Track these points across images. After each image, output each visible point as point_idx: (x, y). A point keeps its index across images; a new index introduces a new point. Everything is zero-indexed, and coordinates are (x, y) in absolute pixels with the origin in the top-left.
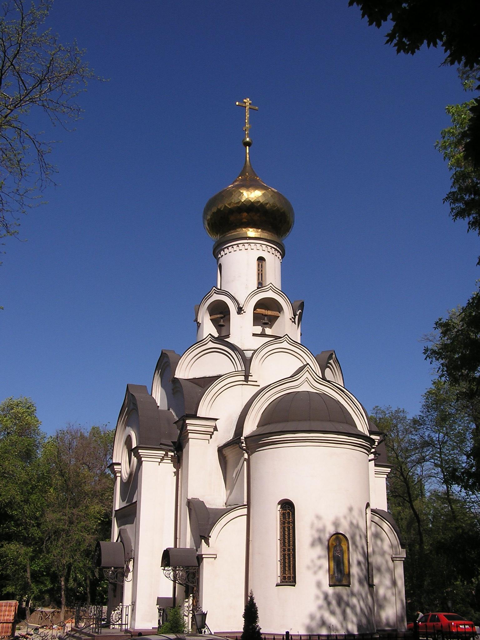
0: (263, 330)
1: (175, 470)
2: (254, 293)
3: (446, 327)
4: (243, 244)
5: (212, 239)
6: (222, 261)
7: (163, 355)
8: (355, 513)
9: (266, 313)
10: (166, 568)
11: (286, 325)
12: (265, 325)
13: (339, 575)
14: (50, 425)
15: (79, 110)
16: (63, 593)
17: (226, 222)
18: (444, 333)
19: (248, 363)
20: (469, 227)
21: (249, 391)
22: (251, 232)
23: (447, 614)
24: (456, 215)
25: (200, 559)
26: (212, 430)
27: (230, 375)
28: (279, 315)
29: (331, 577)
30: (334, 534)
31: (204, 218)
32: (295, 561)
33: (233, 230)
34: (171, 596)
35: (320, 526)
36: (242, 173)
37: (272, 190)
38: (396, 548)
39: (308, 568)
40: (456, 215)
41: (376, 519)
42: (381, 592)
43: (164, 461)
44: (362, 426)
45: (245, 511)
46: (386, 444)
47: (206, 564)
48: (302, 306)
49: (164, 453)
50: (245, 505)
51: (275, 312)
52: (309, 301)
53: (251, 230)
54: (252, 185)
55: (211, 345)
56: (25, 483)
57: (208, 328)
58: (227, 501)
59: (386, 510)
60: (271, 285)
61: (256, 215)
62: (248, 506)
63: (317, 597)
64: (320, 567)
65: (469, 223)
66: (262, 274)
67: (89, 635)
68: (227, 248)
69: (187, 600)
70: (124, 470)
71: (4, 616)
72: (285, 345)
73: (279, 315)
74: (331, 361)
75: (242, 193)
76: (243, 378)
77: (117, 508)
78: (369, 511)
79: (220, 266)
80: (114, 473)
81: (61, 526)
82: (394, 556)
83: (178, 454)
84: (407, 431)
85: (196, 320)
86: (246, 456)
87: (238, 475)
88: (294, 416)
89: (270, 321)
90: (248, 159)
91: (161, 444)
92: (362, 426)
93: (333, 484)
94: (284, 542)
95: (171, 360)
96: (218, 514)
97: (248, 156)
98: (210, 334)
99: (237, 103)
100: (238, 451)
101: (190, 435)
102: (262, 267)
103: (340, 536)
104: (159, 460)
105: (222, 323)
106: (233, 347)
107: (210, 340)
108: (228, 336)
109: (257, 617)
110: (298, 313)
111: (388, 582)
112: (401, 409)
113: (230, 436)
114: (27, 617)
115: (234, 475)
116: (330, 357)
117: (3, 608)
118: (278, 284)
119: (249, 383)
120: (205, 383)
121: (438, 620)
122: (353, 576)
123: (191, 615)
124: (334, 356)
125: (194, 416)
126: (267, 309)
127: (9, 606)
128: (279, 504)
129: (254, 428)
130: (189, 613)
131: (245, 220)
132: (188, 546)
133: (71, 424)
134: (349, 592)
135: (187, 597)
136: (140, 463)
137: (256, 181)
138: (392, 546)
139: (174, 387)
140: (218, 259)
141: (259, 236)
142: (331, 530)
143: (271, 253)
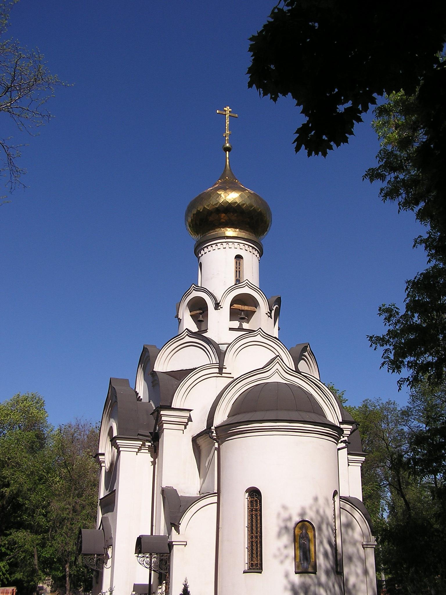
1: (152, 460)
3: (389, 312)
5: (194, 238)
6: (202, 259)
7: (145, 350)
8: (321, 501)
9: (242, 309)
10: (140, 555)
11: (262, 319)
12: (242, 319)
13: (305, 563)
15: (49, 116)
17: (207, 223)
18: (388, 319)
19: (222, 355)
20: (400, 208)
21: (224, 382)
22: (230, 232)
24: (386, 196)
25: (170, 546)
26: (186, 420)
27: (204, 368)
28: (256, 310)
29: (297, 567)
30: (300, 522)
31: (186, 219)
32: (261, 548)
33: (212, 230)
34: (148, 583)
35: (285, 515)
36: (223, 177)
39: (275, 556)
41: (348, 507)
42: (352, 580)
43: (141, 451)
44: (333, 415)
45: (215, 499)
46: (363, 434)
47: (177, 553)
48: (278, 301)
49: (141, 443)
50: (215, 493)
51: (251, 308)
53: (229, 229)
54: (234, 187)
55: (188, 339)
57: (189, 323)
58: (201, 489)
60: (247, 281)
62: (218, 494)
64: (287, 557)
65: (399, 204)
66: (239, 272)
68: (207, 247)
69: (160, 587)
70: (107, 461)
72: (259, 338)
73: (256, 310)
74: (306, 354)
75: (220, 195)
76: (217, 370)
77: (102, 496)
78: (337, 498)
79: (201, 265)
82: (364, 543)
83: (155, 444)
84: (397, 423)
85: (177, 316)
86: (216, 445)
87: (210, 464)
88: (264, 407)
89: (248, 316)
90: (228, 163)
91: (138, 434)
92: (333, 415)
93: (304, 473)
96: (191, 501)
97: (228, 161)
99: (218, 112)
100: (210, 441)
101: (165, 426)
102: (239, 265)
103: (306, 523)
104: (137, 450)
105: (201, 318)
106: (208, 341)
107: (187, 335)
108: (206, 331)
110: (274, 308)
111: (360, 571)
113: (203, 427)
115: (207, 464)
116: (305, 349)
119: (223, 375)
120: (180, 375)
122: (320, 565)
124: (308, 348)
126: (245, 304)
128: (247, 491)
129: (225, 418)
131: (223, 220)
132: (162, 534)
134: (316, 581)
135: (160, 583)
136: (119, 452)
137: (236, 183)
138: (363, 535)
139: (153, 379)
140: (199, 258)
141: (236, 236)
142: (296, 519)
143: (248, 251)
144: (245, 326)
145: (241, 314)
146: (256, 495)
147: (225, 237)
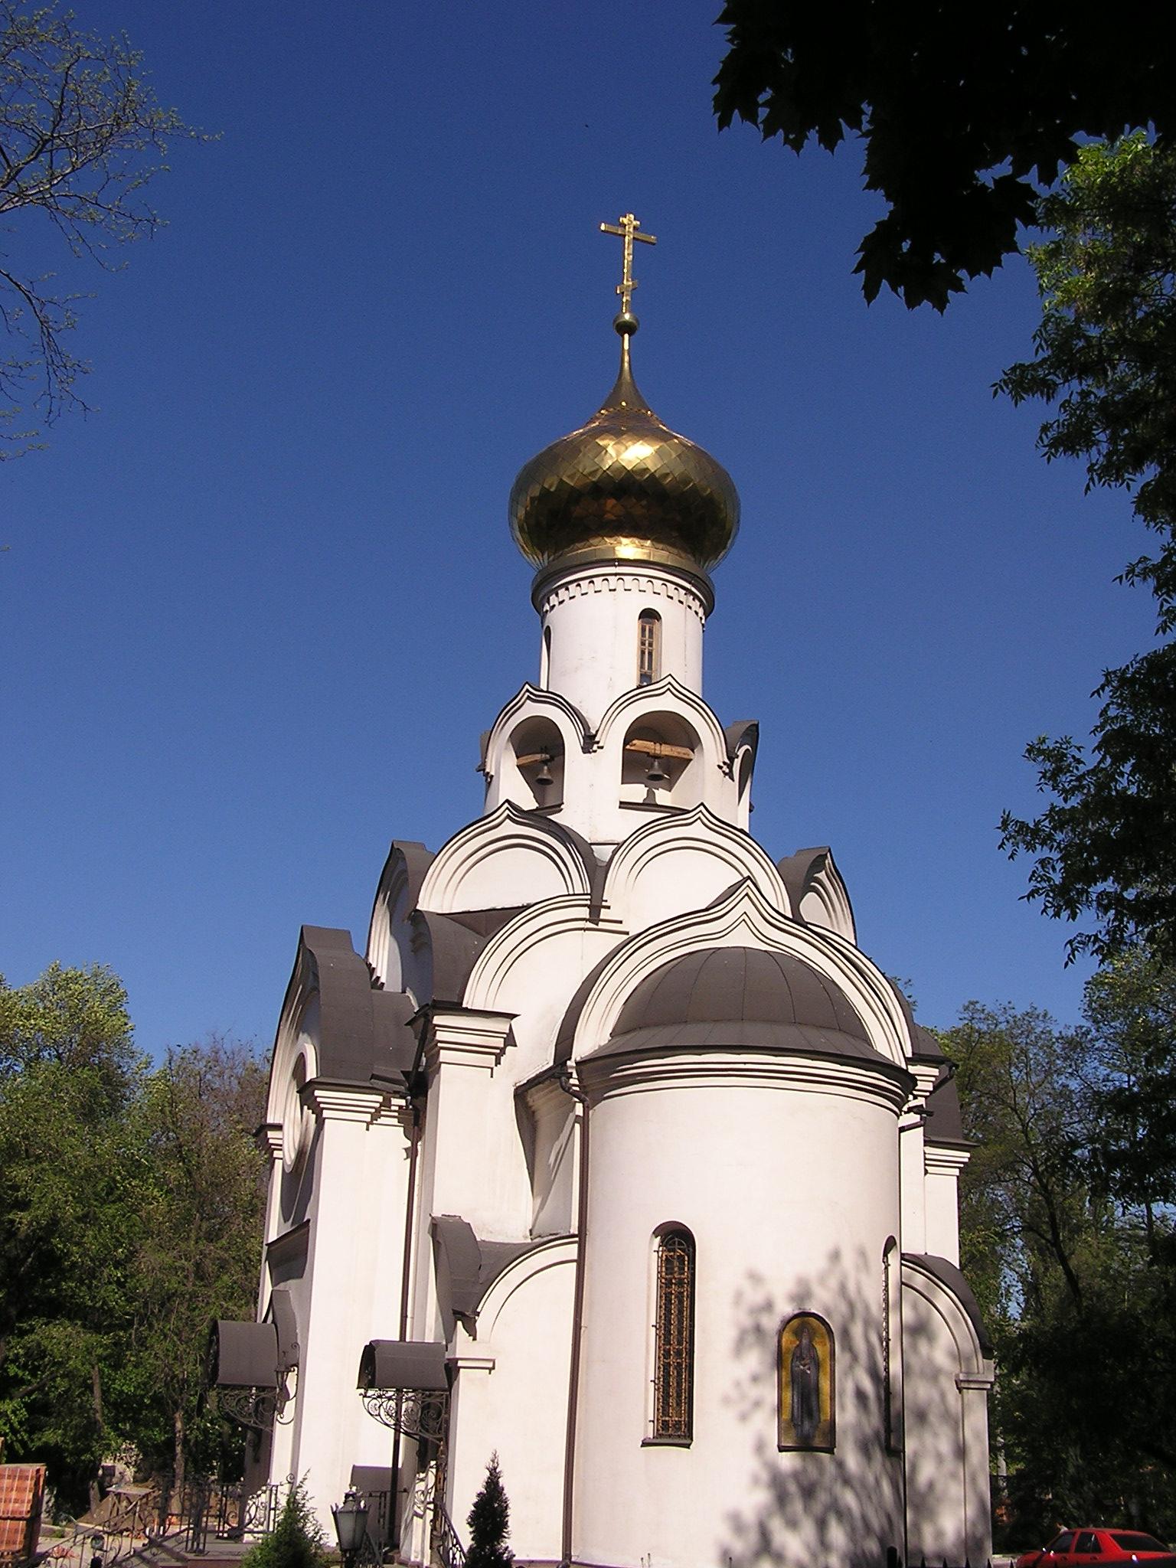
0: (651, 794)
1: (408, 1144)
2: (628, 699)
3: (1055, 761)
4: (605, 577)
7: (395, 855)
8: (848, 1260)
9: (655, 751)
10: (370, 1393)
11: (707, 781)
12: (654, 780)
13: (806, 1424)
14: (157, 1038)
16: (179, 1449)
17: (567, 522)
18: (1052, 777)
21: (602, 944)
22: (628, 548)
23: (1120, 1532)
24: (1055, 444)
25: (452, 1370)
26: (500, 1042)
27: (550, 904)
30: (795, 1316)
31: (512, 512)
34: (390, 1465)
35: (755, 1297)
36: (612, 401)
37: (681, 443)
38: (968, 1360)
39: (726, 1401)
40: (1055, 444)
41: (919, 1280)
42: (927, 1471)
43: (379, 1121)
45: (572, 1251)
46: (964, 1092)
48: (752, 734)
49: (380, 1099)
51: (679, 749)
52: (760, 715)
53: (624, 541)
54: (631, 424)
55: (509, 828)
56: (88, 1175)
57: (512, 785)
59: (955, 1260)
61: (640, 505)
63: (756, 1481)
64: (757, 1404)
65: (1090, 470)
66: (650, 654)
67: (179, 1558)
68: (566, 586)
69: (422, 1475)
70: (287, 1144)
71: (7, 1501)
72: (698, 830)
74: (822, 875)
75: (604, 448)
76: (585, 912)
77: (273, 1235)
78: (894, 1259)
80: (269, 1149)
81: (172, 1284)
82: (962, 1377)
83: (417, 1102)
85: (482, 768)
86: (579, 1109)
88: (707, 1011)
89: (669, 771)
90: (626, 365)
91: (373, 1077)
92: (889, 1040)
93: (806, 1188)
94: (668, 1333)
95: (411, 866)
96: (508, 1256)
97: (626, 358)
98: (507, 801)
99: (603, 227)
100: (563, 1097)
101: (444, 1055)
104: (368, 1118)
105: (545, 775)
106: (564, 835)
107: (508, 817)
108: (557, 808)
109: (505, 1525)
110: (741, 753)
111: (945, 1446)
112: (1040, 1011)
114: (93, 1506)
116: (818, 863)
117: (6, 1482)
118: (691, 678)
119: (602, 925)
120: (487, 924)
121: (1097, 1548)
123: (430, 1515)
124: (828, 861)
125: (456, 1007)
126: (662, 740)
127: (20, 1478)
128: (656, 1233)
129: (605, 1039)
130: (427, 1508)
131: (609, 516)
132: (430, 1338)
133: (218, 1036)
135: (423, 1467)
136: (320, 1123)
138: (958, 1357)
139: (415, 932)
141: (645, 557)
142: (785, 1308)
144: (663, 797)
145: (652, 765)
146: (680, 1244)
147: (614, 560)
